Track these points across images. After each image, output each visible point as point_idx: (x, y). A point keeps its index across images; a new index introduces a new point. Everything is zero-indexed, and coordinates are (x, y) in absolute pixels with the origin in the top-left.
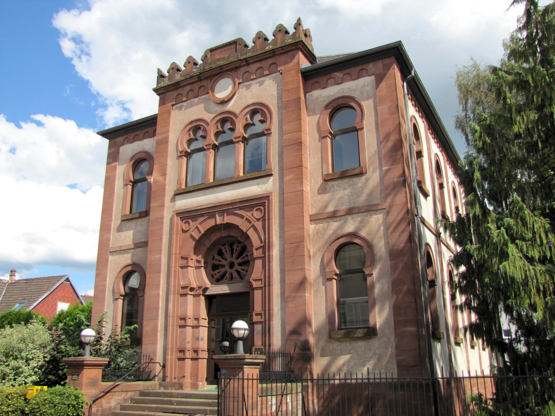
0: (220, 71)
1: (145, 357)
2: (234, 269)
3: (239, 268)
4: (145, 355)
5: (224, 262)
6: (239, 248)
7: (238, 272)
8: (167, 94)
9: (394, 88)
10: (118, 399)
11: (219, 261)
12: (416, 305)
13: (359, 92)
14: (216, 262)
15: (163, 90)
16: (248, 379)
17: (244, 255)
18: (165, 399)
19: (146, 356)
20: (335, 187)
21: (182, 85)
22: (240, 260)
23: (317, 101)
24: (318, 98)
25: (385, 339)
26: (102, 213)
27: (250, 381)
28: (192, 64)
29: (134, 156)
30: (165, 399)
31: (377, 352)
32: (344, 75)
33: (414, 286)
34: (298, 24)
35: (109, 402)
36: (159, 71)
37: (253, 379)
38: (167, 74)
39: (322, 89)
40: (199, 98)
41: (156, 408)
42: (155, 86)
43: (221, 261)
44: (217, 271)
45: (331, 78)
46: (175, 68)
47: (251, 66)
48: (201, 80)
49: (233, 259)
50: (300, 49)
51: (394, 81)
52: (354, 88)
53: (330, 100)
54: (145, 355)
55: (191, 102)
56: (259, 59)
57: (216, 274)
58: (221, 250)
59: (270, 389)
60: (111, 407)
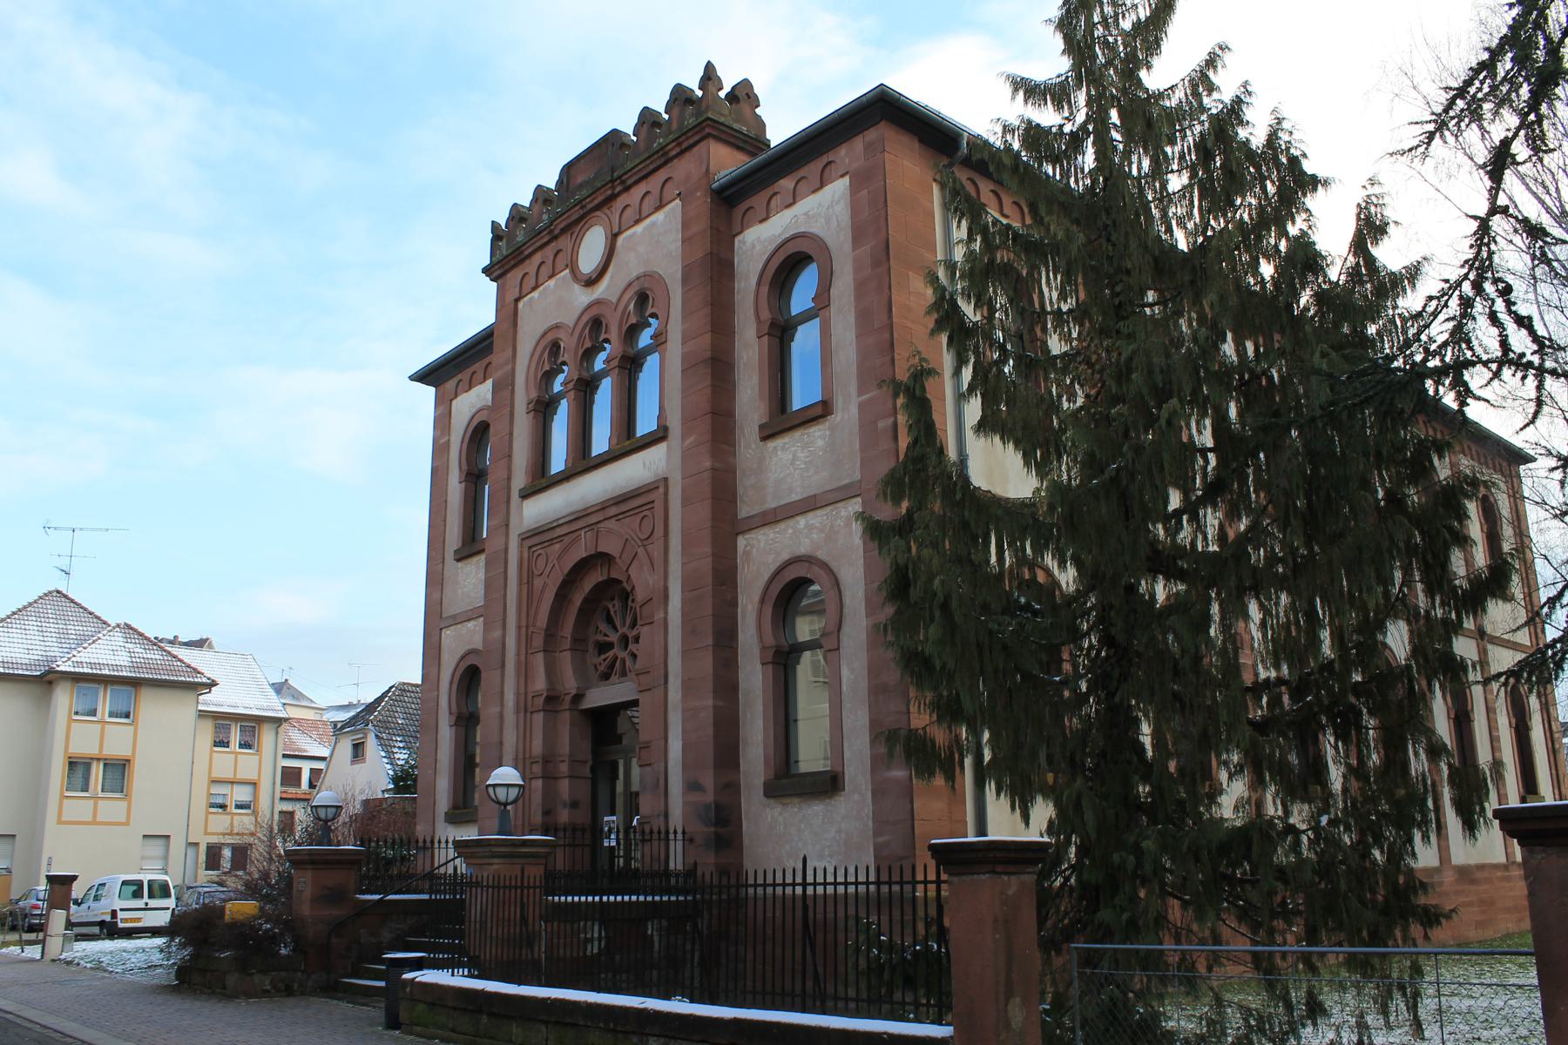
0: (582, 212)
1: (443, 845)
4: (443, 840)
5: (613, 637)
8: (509, 275)
9: (882, 199)
13: (823, 220)
14: (601, 638)
16: (505, 887)
19: (675, 832)
20: (779, 453)
24: (754, 246)
25: (856, 797)
29: (472, 418)
31: (843, 826)
34: (709, 76)
37: (534, 888)
43: (607, 636)
44: (603, 657)
45: (776, 194)
50: (709, 136)
51: (883, 183)
53: (771, 248)
54: (443, 840)
56: (642, 174)
59: (854, 898)
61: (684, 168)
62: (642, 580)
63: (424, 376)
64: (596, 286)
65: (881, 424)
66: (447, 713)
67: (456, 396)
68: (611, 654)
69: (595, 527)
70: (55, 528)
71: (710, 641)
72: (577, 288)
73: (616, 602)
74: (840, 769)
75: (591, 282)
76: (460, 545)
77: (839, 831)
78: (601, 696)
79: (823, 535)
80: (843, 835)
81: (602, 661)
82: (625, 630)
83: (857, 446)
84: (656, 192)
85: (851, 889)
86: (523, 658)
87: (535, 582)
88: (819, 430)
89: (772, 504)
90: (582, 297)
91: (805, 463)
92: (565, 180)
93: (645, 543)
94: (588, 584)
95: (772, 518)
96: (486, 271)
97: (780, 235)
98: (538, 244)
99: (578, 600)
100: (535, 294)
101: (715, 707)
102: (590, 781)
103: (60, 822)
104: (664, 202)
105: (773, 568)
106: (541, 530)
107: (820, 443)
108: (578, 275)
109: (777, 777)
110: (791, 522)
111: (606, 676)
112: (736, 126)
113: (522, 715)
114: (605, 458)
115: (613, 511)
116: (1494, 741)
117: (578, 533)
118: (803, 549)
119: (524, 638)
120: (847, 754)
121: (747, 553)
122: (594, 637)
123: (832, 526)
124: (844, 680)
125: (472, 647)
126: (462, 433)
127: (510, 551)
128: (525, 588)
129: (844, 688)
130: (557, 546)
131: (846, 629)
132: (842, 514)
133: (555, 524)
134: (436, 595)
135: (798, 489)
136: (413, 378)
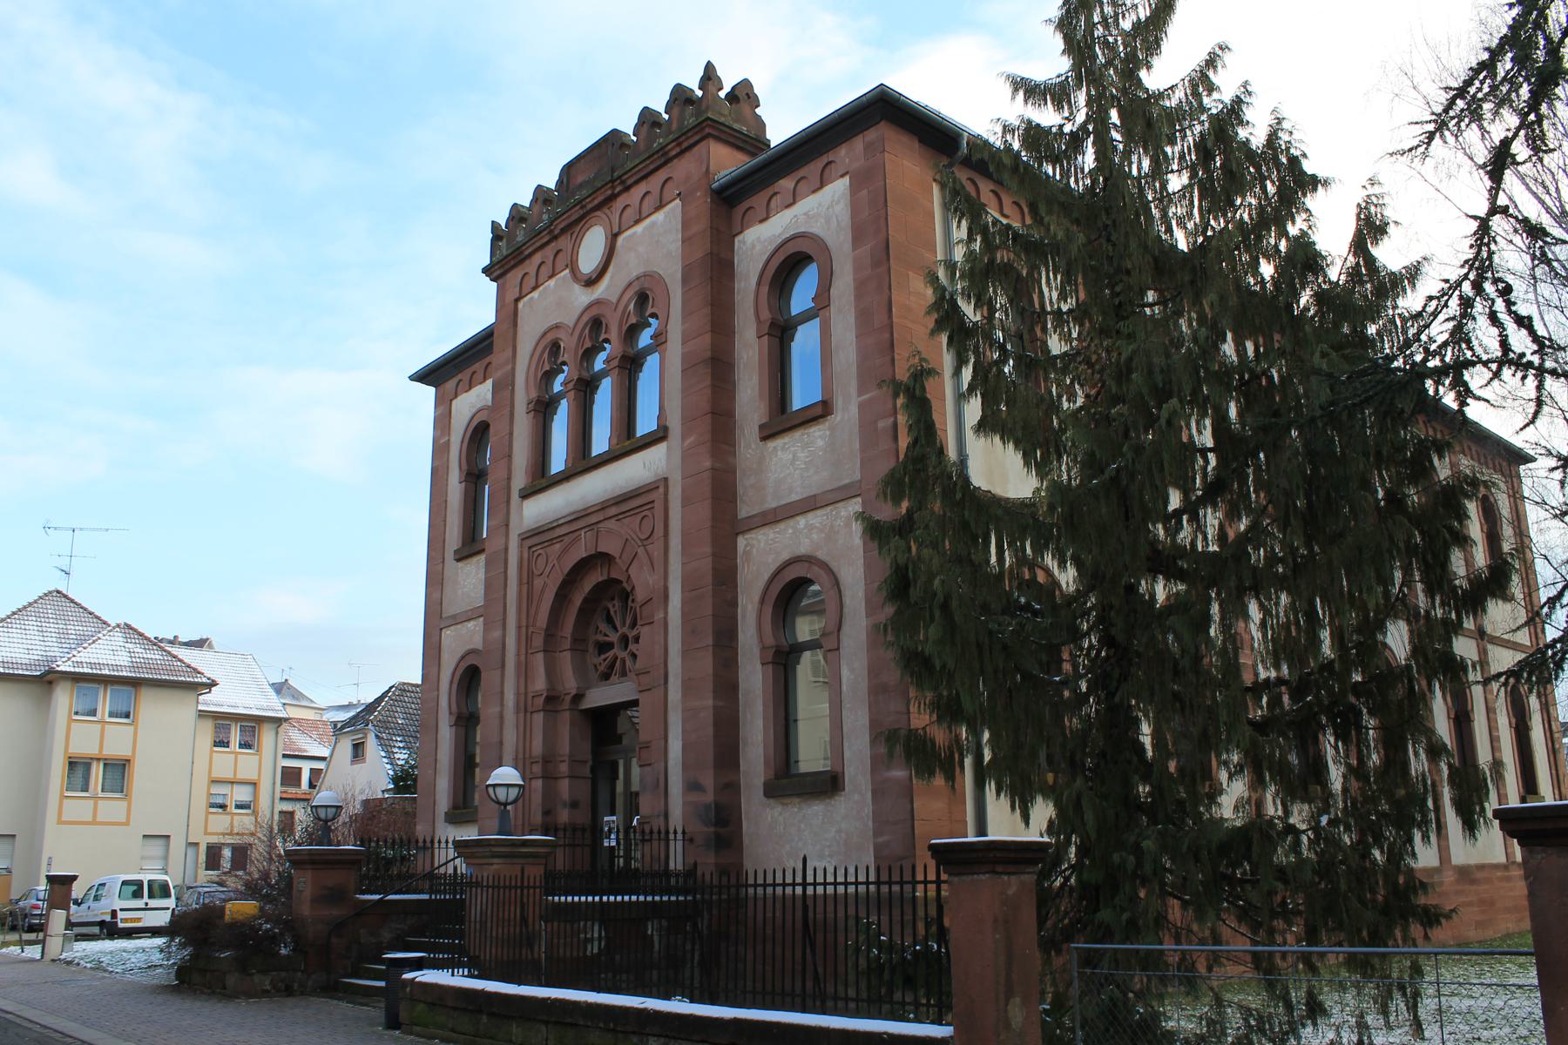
0: (581, 212)
1: (443, 845)
4: (443, 840)
5: (613, 637)
9: (882, 199)
13: (823, 220)
14: (601, 638)
15: (513, 258)
19: (675, 832)
24: (753, 246)
25: (856, 797)
27: (531, 891)
32: (796, 184)
34: (709, 76)
42: (487, 261)
43: (607, 636)
44: (603, 657)
45: (776, 194)
47: (632, 190)
48: (556, 238)
50: (709, 136)
51: (883, 183)
54: (443, 840)
56: (642, 174)
59: (854, 898)
61: (684, 168)
62: (642, 580)
63: (424, 376)
64: (596, 286)
65: (881, 424)
66: (447, 713)
67: (456, 397)
68: (611, 654)
69: (595, 527)
70: (55, 528)
72: (577, 288)
73: (616, 602)
74: (840, 770)
75: (591, 282)
77: (839, 831)
78: (601, 696)
80: (843, 835)
81: (602, 661)
82: (625, 630)
83: (857, 446)
84: (656, 190)
86: (523, 658)
87: (535, 582)
88: (819, 430)
89: (772, 504)
90: (582, 297)
91: (805, 463)
92: (565, 180)
93: (645, 543)
95: (772, 518)
96: (486, 271)
97: (780, 235)
98: (538, 244)
99: (578, 600)
100: (535, 294)
101: (715, 707)
103: (60, 822)
106: (541, 530)
107: (820, 443)
108: (578, 275)
110: (791, 522)
111: (606, 676)
112: (736, 126)
113: (522, 715)
114: (605, 458)
115: (613, 511)
116: (1494, 741)
117: (578, 533)
118: (803, 549)
119: (524, 637)
120: (847, 754)
121: (747, 553)
124: (844, 680)
125: (471, 647)
128: (525, 588)
129: (844, 688)
131: (846, 629)
133: (555, 524)
136: (413, 378)
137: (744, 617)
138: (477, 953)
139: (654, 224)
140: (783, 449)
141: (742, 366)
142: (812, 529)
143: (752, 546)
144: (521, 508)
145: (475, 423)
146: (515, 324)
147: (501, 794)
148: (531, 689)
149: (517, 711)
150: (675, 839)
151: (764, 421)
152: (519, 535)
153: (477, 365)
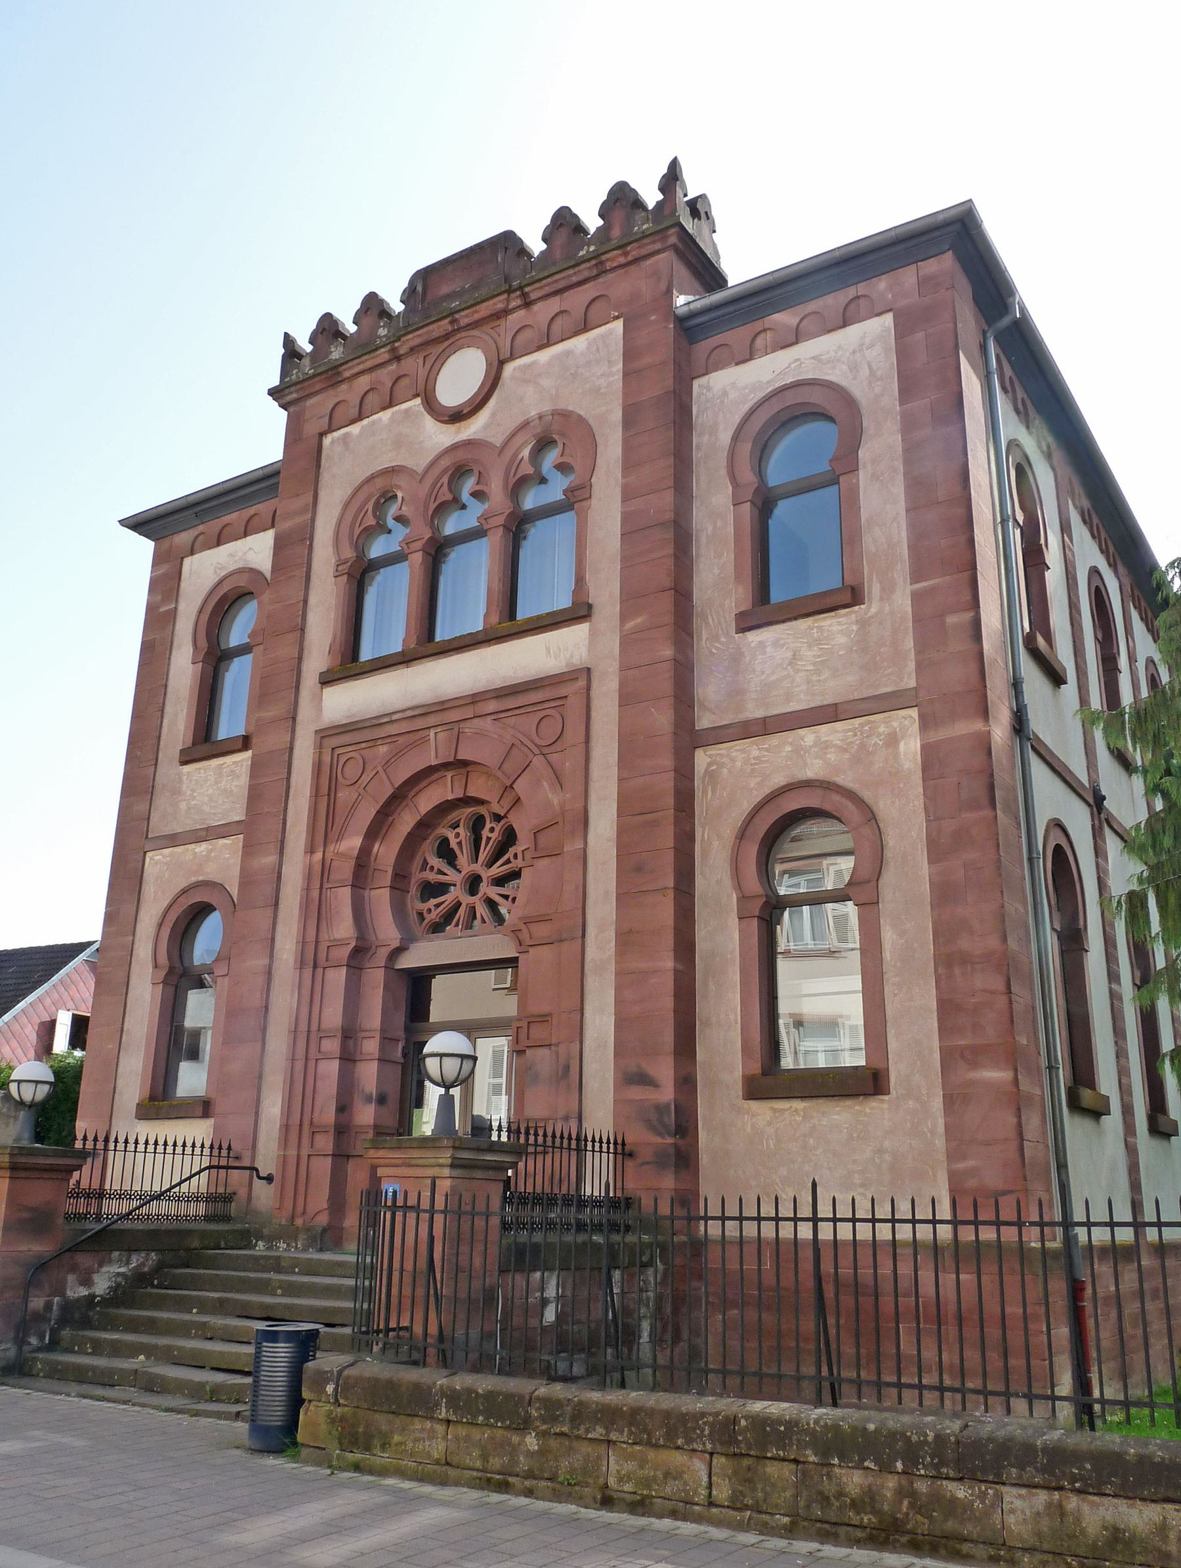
1: (121, 1146)
2: (480, 895)
3: (493, 892)
4: (121, 1140)
5: (452, 876)
6: (494, 836)
7: (492, 905)
10: (118, 1274)
11: (440, 872)
12: (1011, 1002)
13: (845, 367)
14: (432, 877)
15: (296, 391)
17: (509, 855)
18: (252, 1275)
21: (347, 374)
22: (497, 870)
23: (722, 402)
24: (725, 393)
26: (129, 744)
28: (375, 312)
29: (220, 582)
30: (252, 1275)
33: (1004, 939)
34: (672, 178)
35: (87, 1282)
36: (288, 341)
38: (309, 348)
39: (737, 364)
40: (397, 408)
41: (221, 1301)
42: (275, 382)
44: (433, 901)
46: (328, 328)
48: (398, 358)
49: (478, 868)
51: (951, 325)
52: (832, 354)
53: (760, 395)
54: (121, 1140)
55: (374, 422)
57: (429, 911)
58: (445, 841)
60: (93, 1296)
63: (140, 524)
64: (463, 423)
65: (951, 620)
66: (150, 965)
67: (192, 553)
71: (671, 883)
73: (460, 830)
74: (881, 1066)
75: (457, 416)
76: (189, 743)
77: (880, 1151)
79: (847, 756)
80: (887, 1157)
81: (434, 908)
84: (578, 313)
85: (945, 1232)
86: (315, 894)
87: (340, 795)
88: (840, 624)
90: (440, 437)
91: (814, 664)
92: (419, 288)
93: (546, 751)
94: (427, 800)
95: (173, 840)
96: (273, 393)
97: (768, 382)
98: (369, 364)
99: (406, 822)
100: (355, 429)
101: (676, 970)
102: (400, 1067)
104: (334, 426)
105: (758, 796)
109: (152, 1098)
110: (790, 736)
111: (437, 928)
113: (308, 972)
114: (480, 637)
115: (492, 706)
117: (425, 732)
118: (813, 769)
120: (893, 1045)
121: (711, 775)
122: (418, 876)
123: (862, 746)
126: (198, 602)
127: (297, 752)
129: (887, 955)
130: (383, 749)
131: (888, 878)
132: (881, 730)
134: (140, 808)
135: (802, 696)
136: (123, 523)
137: (705, 855)
138: (405, 1323)
139: (568, 353)
140: (776, 644)
141: (704, 539)
142: (827, 748)
143: (721, 765)
144: (319, 699)
145: (225, 588)
146: (318, 465)
147: (28, 1094)
148: (324, 936)
149: (301, 964)
150: (593, 1151)
151: (742, 609)
152: (317, 732)
153: (234, 516)
